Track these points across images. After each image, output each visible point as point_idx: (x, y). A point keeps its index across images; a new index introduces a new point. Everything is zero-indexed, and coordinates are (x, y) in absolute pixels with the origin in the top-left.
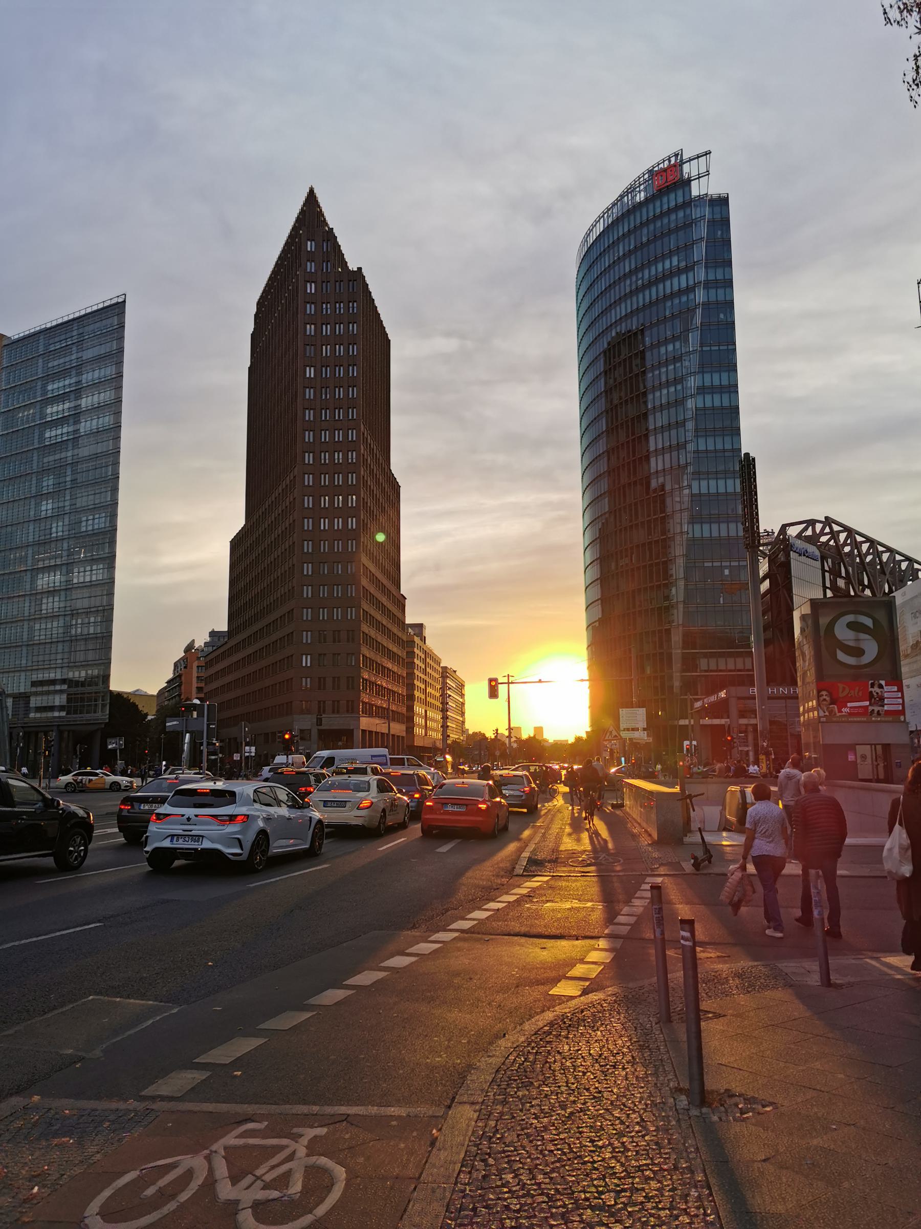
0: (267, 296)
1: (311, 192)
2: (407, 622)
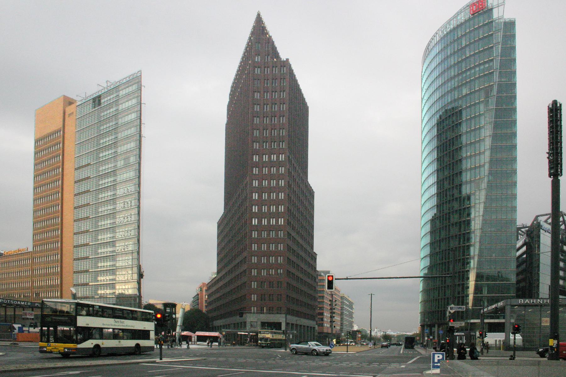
1: (259, 20)
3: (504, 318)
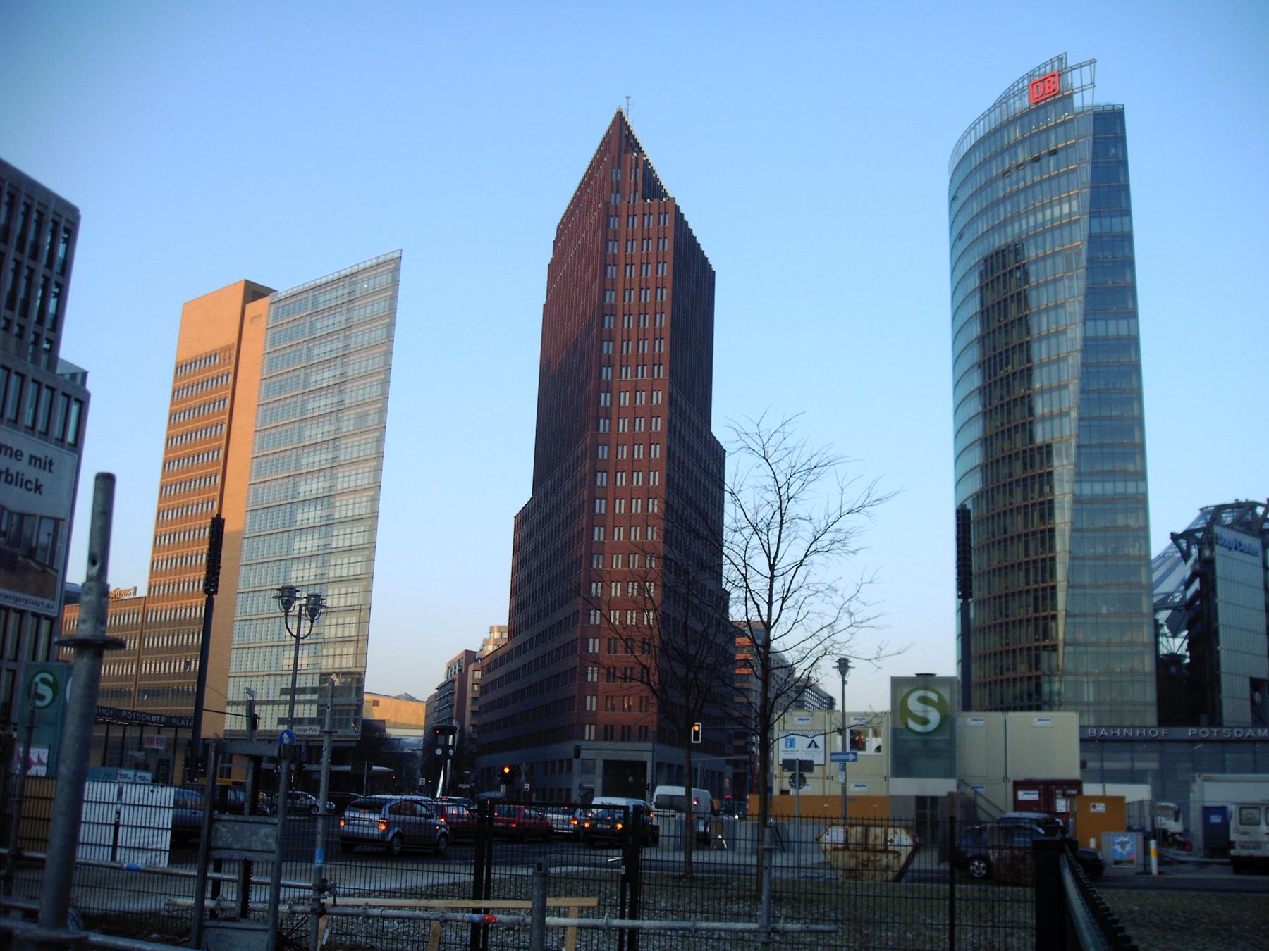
0: (593, 173)
3: (949, 774)
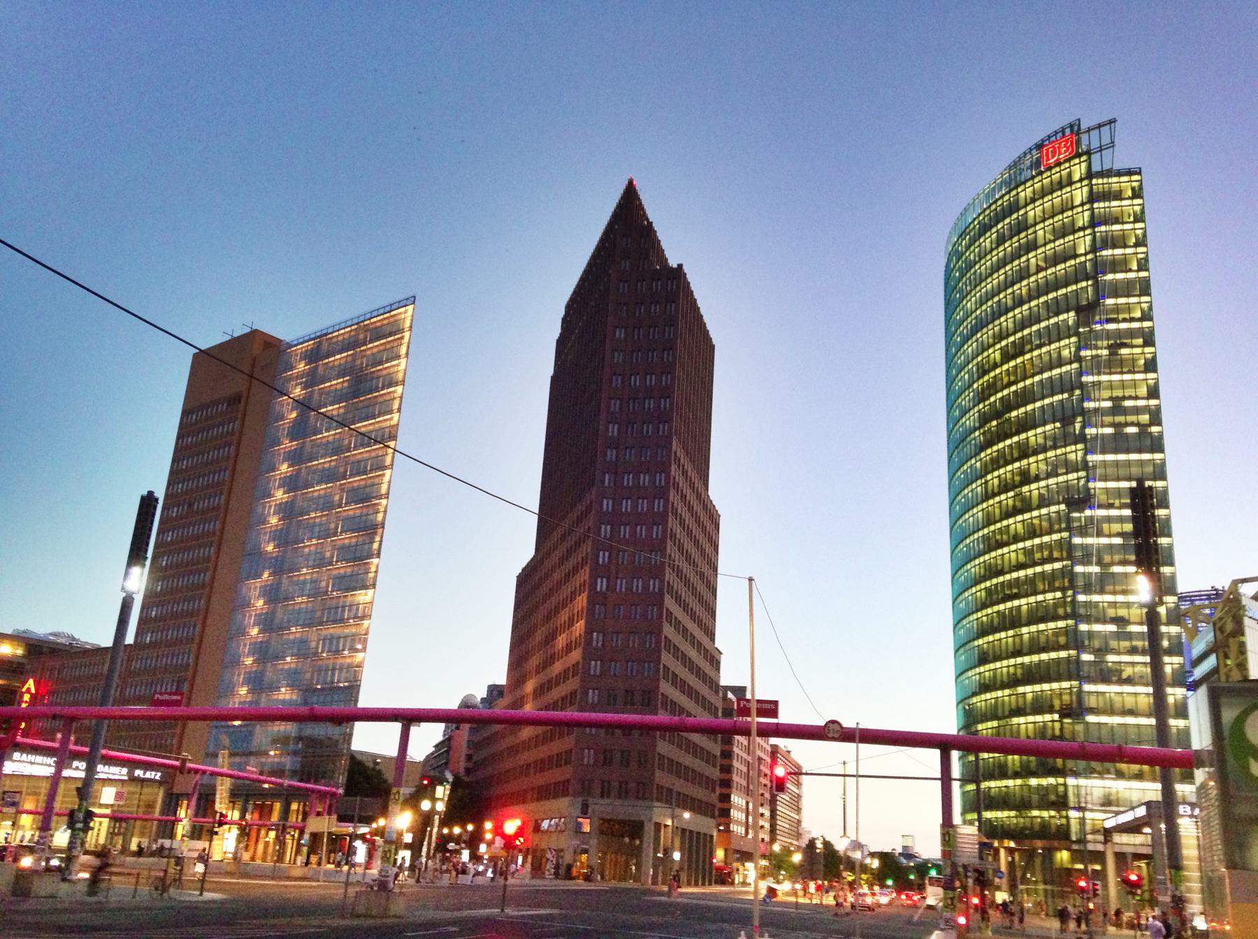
1: (631, 183)
2: (723, 682)
